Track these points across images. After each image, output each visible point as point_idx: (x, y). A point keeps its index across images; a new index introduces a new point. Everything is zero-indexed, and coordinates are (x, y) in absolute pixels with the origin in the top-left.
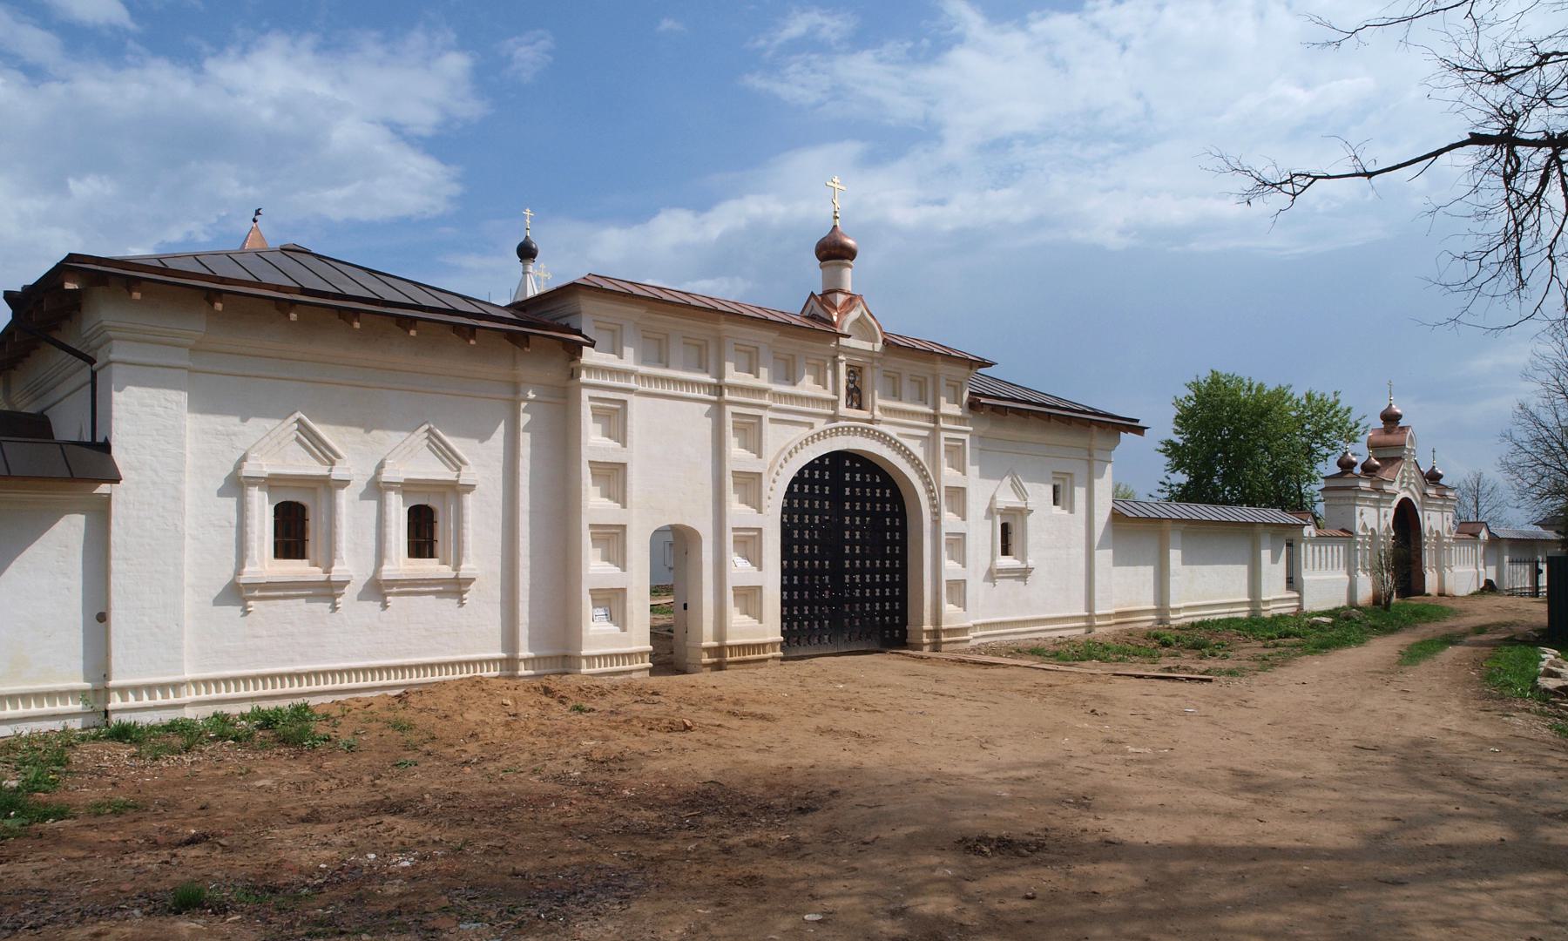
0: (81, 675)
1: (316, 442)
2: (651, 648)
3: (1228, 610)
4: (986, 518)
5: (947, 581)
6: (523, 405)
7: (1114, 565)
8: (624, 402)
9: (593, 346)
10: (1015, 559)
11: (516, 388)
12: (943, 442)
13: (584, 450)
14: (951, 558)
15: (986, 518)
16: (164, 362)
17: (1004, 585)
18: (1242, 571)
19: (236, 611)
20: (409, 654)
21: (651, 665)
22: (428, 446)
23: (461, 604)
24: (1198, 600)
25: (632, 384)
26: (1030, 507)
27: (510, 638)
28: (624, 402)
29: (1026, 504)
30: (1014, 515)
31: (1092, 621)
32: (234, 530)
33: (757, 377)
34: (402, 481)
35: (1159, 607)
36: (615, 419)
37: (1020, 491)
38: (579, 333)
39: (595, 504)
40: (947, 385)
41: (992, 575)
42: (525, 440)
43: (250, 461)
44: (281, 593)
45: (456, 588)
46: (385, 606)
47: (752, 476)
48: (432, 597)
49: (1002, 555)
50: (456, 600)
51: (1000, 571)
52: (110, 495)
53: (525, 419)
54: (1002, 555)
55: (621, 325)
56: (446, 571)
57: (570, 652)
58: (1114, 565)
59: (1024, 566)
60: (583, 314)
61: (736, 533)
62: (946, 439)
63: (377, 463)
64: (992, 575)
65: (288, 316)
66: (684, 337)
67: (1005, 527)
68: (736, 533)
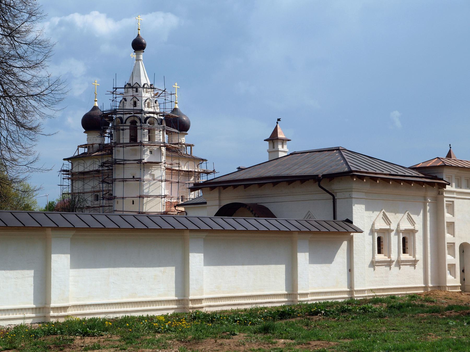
0: (32, 302)
1: (386, 218)
2: (460, 285)
3: (21, 316)
4: (370, 234)
5: (448, 264)
6: (428, 204)
7: (205, 265)
8: (453, 202)
9: (449, 185)
10: (385, 256)
11: (425, 198)
12: (445, 203)
13: (445, 219)
14: (449, 254)
15: (370, 234)
16: (361, 197)
17: (381, 269)
18: (282, 269)
19: (372, 269)
20: (405, 284)
21: (461, 290)
22: (407, 218)
23: (415, 268)
24: (416, 284)
25: (455, 196)
26: (416, 229)
27: (426, 281)
28: (453, 202)
29: (414, 228)
30: (409, 233)
31: (353, 294)
32: (372, 245)
33: (452, 187)
34: (379, 229)
35: (181, 298)
36: (451, 206)
37: (412, 221)
38: (442, 180)
39: (448, 238)
40: (446, 177)
41: (373, 264)
42: (428, 214)
43: (375, 225)
44: (381, 264)
45: (414, 263)
46: (400, 269)
47: (451, 223)
48: (409, 266)
49: (378, 253)
50: (389, 268)
51: (403, 261)
52: (353, 236)
53: (428, 208)
54: (378, 253)
55: (451, 176)
56: (411, 258)
57: (441, 285)
58: (205, 265)
59: (389, 259)
60: (444, 173)
61: (448, 245)
62: (446, 201)
63: (397, 224)
64: (373, 264)
65: (423, 186)
66: (465, 177)
67: (379, 239)
68: (448, 245)
